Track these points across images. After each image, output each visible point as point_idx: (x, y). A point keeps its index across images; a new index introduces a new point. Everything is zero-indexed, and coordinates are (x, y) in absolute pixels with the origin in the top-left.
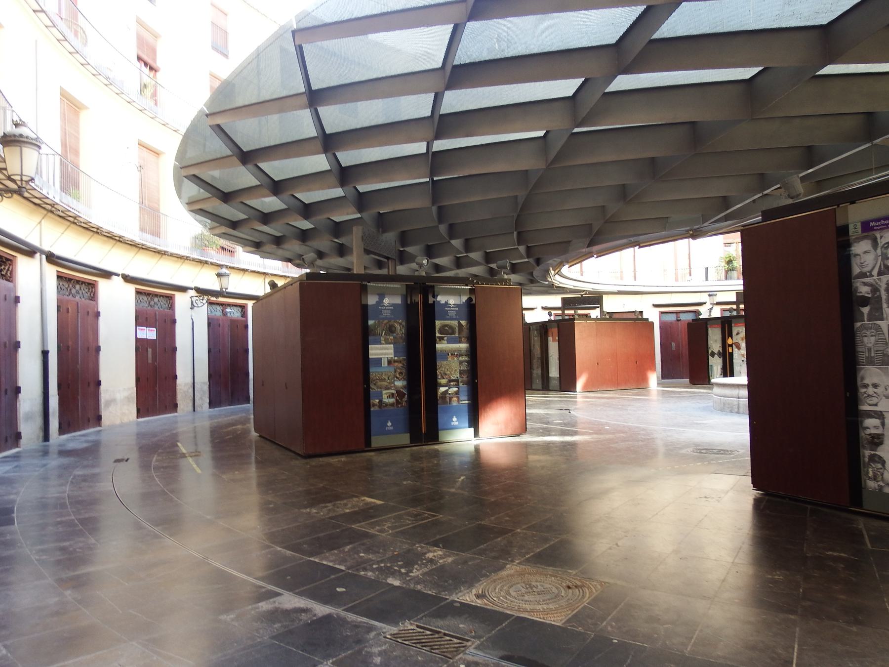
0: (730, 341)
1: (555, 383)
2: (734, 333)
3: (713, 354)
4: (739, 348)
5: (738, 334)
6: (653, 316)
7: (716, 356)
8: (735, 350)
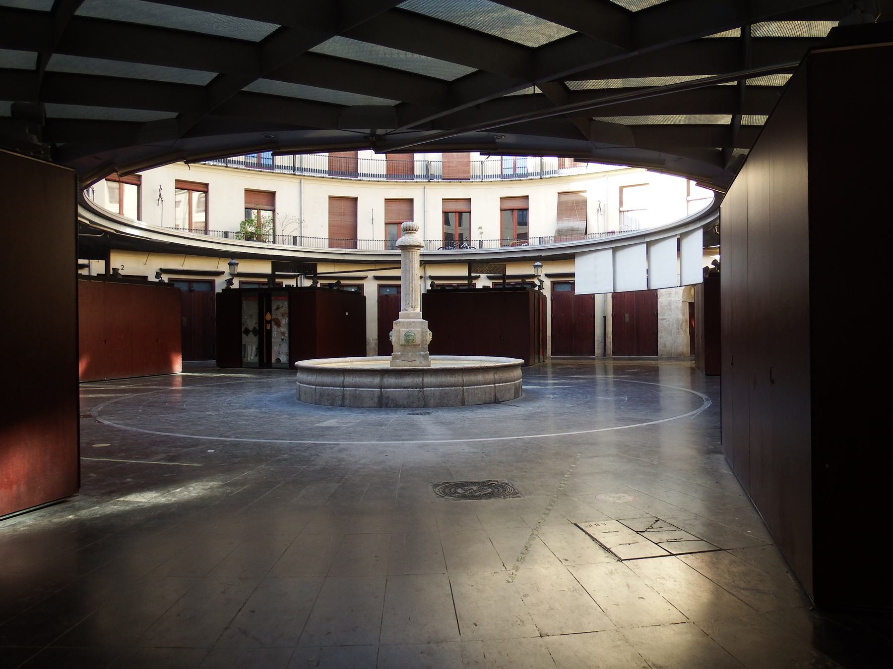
0: (268, 317)
2: (274, 307)
3: (247, 332)
4: (278, 324)
5: (278, 309)
7: (251, 334)
8: (275, 327)
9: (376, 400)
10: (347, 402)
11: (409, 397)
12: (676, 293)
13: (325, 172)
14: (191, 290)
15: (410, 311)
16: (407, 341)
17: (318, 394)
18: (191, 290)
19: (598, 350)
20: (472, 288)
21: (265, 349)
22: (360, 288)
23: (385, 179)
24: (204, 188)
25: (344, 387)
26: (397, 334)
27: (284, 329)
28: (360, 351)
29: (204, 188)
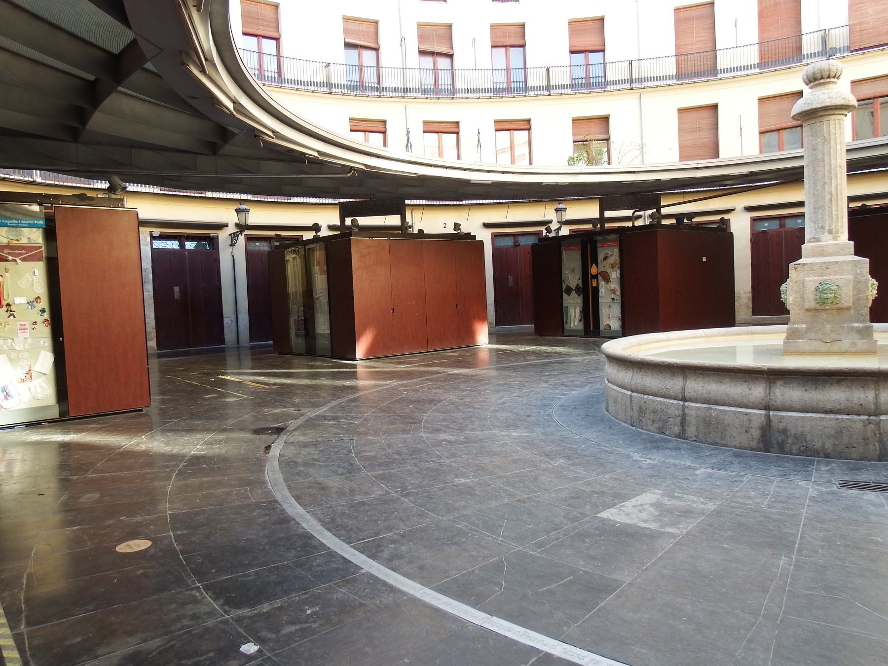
0: (594, 270)
1: (324, 343)
2: (601, 257)
3: (569, 291)
4: (607, 280)
5: (605, 258)
6: (485, 236)
7: (573, 293)
8: (602, 283)
9: (756, 433)
10: (691, 431)
11: (839, 433)
13: (670, 77)
14: (516, 245)
15: (827, 240)
16: (823, 302)
17: (636, 408)
18: (516, 245)
21: (591, 313)
22: (725, 223)
23: (757, 70)
24: (526, 125)
25: (684, 399)
26: (798, 287)
27: (615, 285)
28: (721, 315)
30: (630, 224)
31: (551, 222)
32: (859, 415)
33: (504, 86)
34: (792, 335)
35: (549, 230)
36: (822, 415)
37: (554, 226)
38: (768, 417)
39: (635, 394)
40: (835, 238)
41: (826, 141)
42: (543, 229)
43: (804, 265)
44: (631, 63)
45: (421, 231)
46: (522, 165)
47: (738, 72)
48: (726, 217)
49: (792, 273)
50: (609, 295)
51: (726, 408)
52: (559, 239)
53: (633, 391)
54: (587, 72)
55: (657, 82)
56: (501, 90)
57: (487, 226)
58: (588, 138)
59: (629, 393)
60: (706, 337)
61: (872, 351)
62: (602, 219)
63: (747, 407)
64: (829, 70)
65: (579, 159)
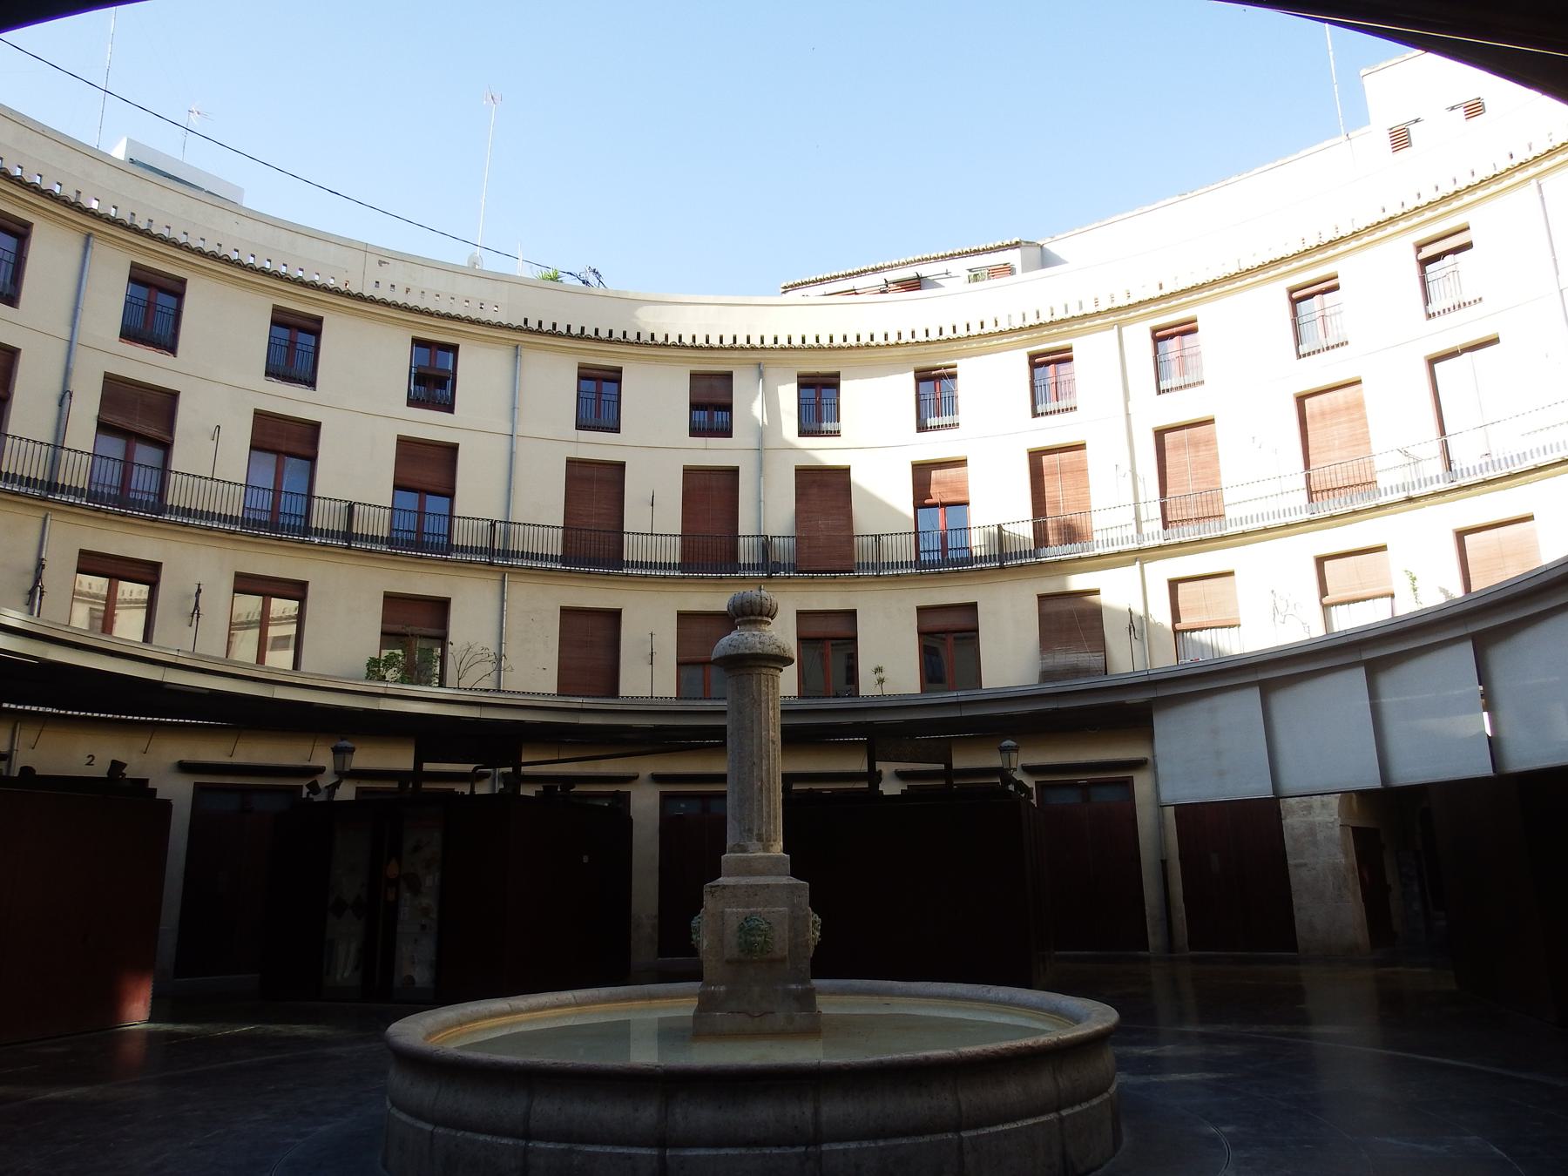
0: (392, 870)
4: (416, 889)
6: (178, 791)
12: (1324, 806)
13: (553, 559)
16: (747, 947)
19: (1155, 939)
20: (874, 795)
24: (297, 590)
25: (528, 1136)
26: (719, 918)
27: (428, 901)
29: (297, 590)
30: (465, 789)
31: (321, 770)
32: (793, 1146)
33: (265, 517)
34: (707, 1004)
35: (314, 788)
36: (743, 1151)
37: (324, 781)
38: (662, 1158)
39: (440, 1130)
40: (766, 849)
41: (757, 703)
42: (304, 783)
43: (725, 887)
44: (493, 525)
45: (27, 771)
46: (280, 660)
47: (651, 574)
48: (623, 788)
49: (708, 901)
50: (416, 911)
51: (597, 1149)
52: (332, 806)
53: (436, 1124)
54: (421, 523)
55: (531, 565)
56: (258, 524)
57: (185, 768)
58: (409, 630)
59: (429, 1127)
60: (577, 1004)
61: (813, 1029)
62: (417, 774)
63: (630, 1144)
64: (762, 605)
65: (390, 662)
